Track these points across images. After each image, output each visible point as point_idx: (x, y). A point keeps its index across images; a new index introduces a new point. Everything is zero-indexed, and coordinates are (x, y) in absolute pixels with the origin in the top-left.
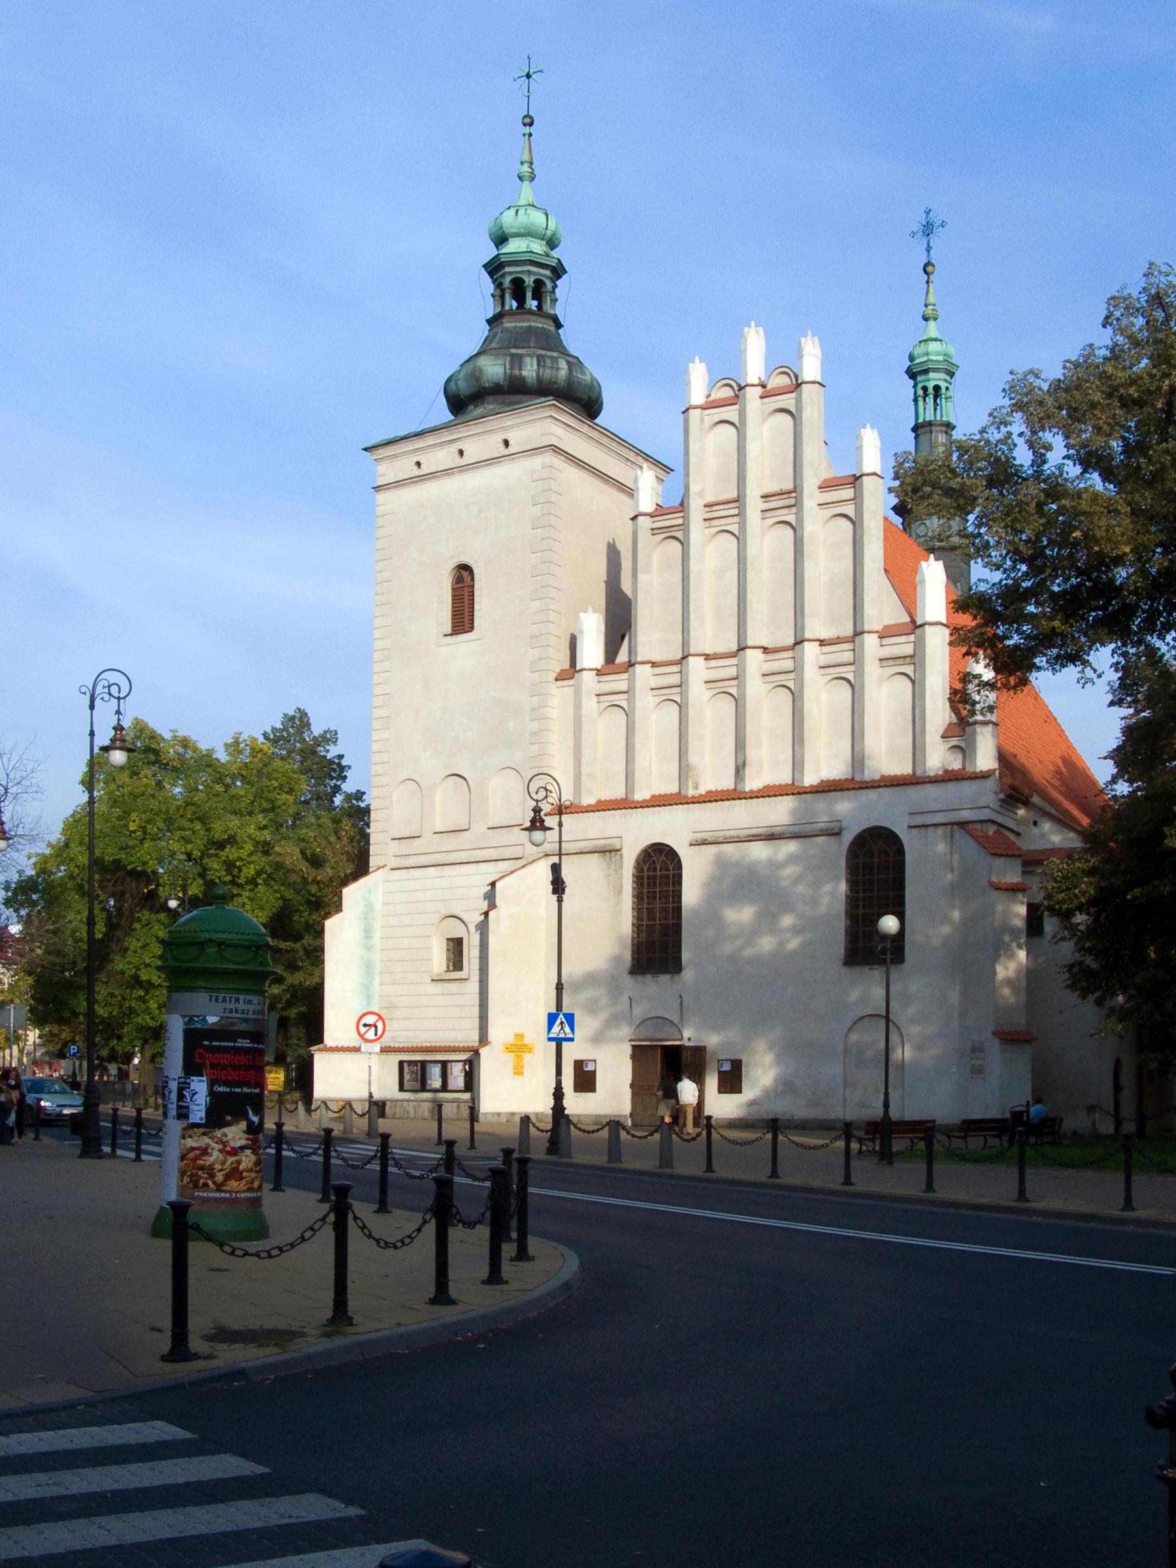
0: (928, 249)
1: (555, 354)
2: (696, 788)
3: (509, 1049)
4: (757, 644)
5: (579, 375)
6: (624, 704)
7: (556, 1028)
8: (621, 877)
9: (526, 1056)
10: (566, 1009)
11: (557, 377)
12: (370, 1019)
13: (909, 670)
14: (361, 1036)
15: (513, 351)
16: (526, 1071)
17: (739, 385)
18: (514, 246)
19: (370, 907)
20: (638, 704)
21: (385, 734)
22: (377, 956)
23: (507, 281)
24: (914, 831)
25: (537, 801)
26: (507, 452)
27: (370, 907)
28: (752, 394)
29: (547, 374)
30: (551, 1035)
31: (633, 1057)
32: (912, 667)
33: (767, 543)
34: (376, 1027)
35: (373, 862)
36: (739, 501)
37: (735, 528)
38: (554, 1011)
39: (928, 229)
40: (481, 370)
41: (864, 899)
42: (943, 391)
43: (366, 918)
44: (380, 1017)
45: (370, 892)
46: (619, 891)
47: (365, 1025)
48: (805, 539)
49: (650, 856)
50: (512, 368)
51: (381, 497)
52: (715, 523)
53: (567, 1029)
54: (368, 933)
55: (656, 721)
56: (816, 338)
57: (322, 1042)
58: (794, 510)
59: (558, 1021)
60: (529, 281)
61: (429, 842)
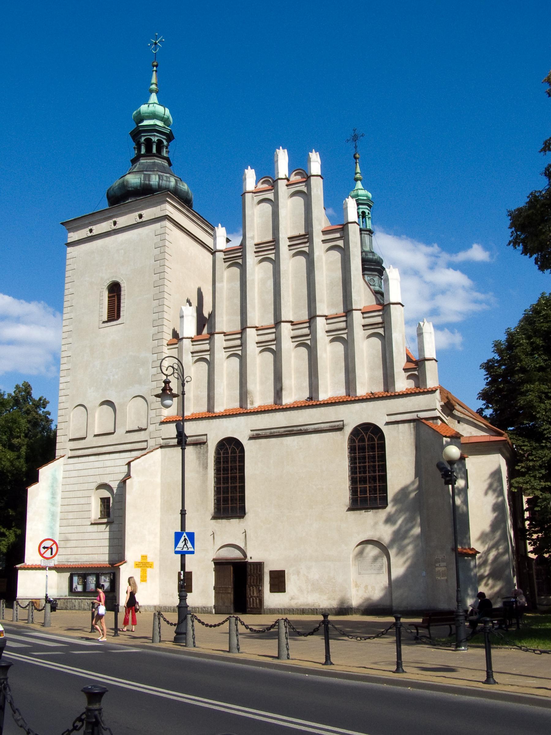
0: (356, 147)
1: (168, 175)
2: (252, 403)
3: (137, 565)
4: (287, 320)
5: (181, 186)
6: (208, 357)
7: (181, 544)
8: (207, 459)
9: (149, 570)
10: (188, 530)
11: (169, 186)
12: (48, 544)
13: (381, 331)
14: (42, 555)
15: (145, 172)
16: (148, 578)
17: (273, 180)
18: (146, 123)
19: (55, 479)
20: (216, 356)
21: (68, 379)
22: (59, 509)
23: (143, 139)
24: (390, 426)
25: (167, 376)
26: (141, 220)
27: (55, 479)
28: (282, 184)
29: (164, 183)
30: (177, 549)
31: (216, 570)
32: (383, 329)
33: (291, 266)
34: (52, 549)
35: (58, 453)
36: (275, 241)
37: (272, 256)
38: (179, 531)
39: (355, 138)
40: (127, 181)
41: (360, 467)
42: (367, 214)
43: (52, 486)
44: (55, 543)
45: (55, 471)
46: (206, 467)
47: (44, 548)
48: (315, 259)
49: (224, 445)
50: (145, 180)
51: (69, 249)
52: (261, 254)
53: (189, 544)
54: (53, 495)
55: (226, 368)
56: (318, 153)
57: (24, 562)
58: (308, 244)
59: (183, 539)
60: (155, 139)
61: (90, 441)
